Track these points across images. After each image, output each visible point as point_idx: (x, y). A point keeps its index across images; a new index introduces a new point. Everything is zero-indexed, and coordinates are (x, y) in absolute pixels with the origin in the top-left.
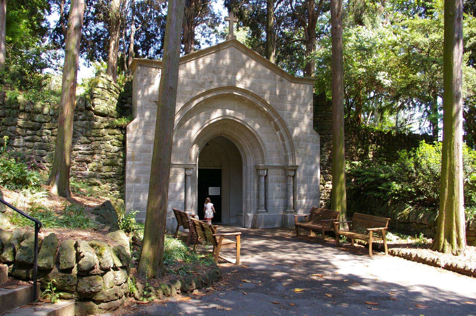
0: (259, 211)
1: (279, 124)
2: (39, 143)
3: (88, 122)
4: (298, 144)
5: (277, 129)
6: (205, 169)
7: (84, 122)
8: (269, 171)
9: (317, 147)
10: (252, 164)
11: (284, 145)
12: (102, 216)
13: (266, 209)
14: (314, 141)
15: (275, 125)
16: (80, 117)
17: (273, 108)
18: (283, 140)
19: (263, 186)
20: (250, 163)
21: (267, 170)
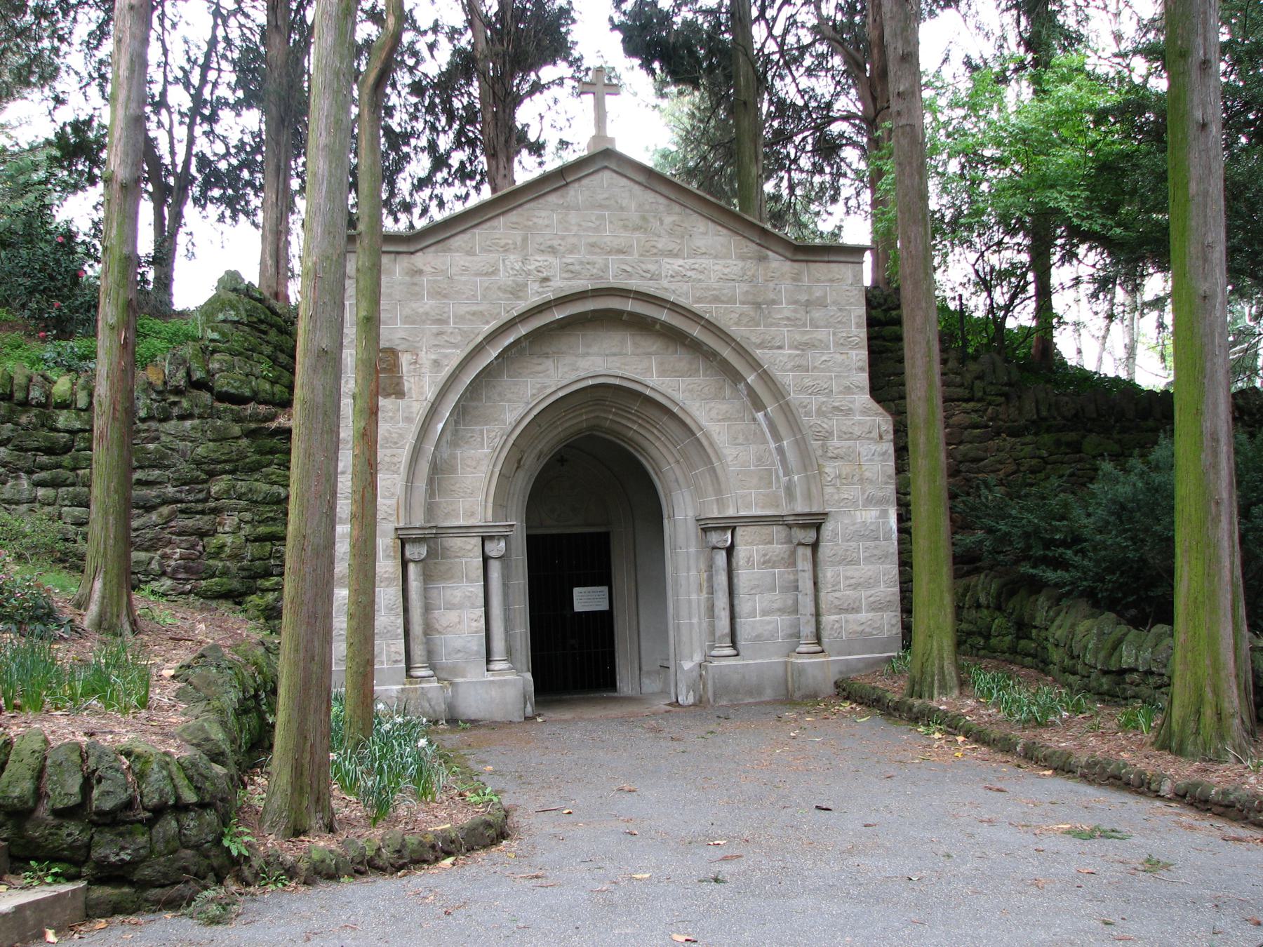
0: (714, 653)
1: (760, 390)
2: (71, 489)
3: (197, 421)
4: (825, 448)
5: (758, 405)
6: (559, 536)
7: (188, 423)
8: (739, 531)
9: (884, 453)
10: (691, 513)
11: (780, 450)
12: (191, 684)
13: (734, 644)
14: (875, 434)
15: (751, 392)
16: (176, 411)
17: (738, 343)
18: (777, 437)
19: (722, 579)
20: (682, 512)
21: (734, 529)
